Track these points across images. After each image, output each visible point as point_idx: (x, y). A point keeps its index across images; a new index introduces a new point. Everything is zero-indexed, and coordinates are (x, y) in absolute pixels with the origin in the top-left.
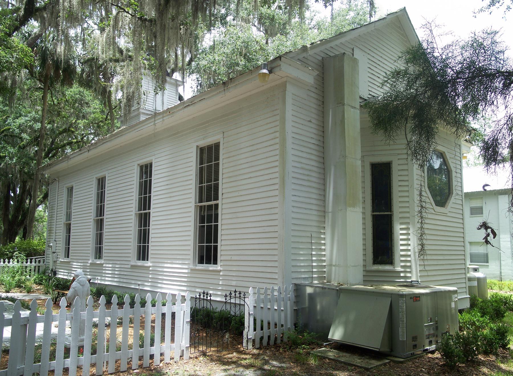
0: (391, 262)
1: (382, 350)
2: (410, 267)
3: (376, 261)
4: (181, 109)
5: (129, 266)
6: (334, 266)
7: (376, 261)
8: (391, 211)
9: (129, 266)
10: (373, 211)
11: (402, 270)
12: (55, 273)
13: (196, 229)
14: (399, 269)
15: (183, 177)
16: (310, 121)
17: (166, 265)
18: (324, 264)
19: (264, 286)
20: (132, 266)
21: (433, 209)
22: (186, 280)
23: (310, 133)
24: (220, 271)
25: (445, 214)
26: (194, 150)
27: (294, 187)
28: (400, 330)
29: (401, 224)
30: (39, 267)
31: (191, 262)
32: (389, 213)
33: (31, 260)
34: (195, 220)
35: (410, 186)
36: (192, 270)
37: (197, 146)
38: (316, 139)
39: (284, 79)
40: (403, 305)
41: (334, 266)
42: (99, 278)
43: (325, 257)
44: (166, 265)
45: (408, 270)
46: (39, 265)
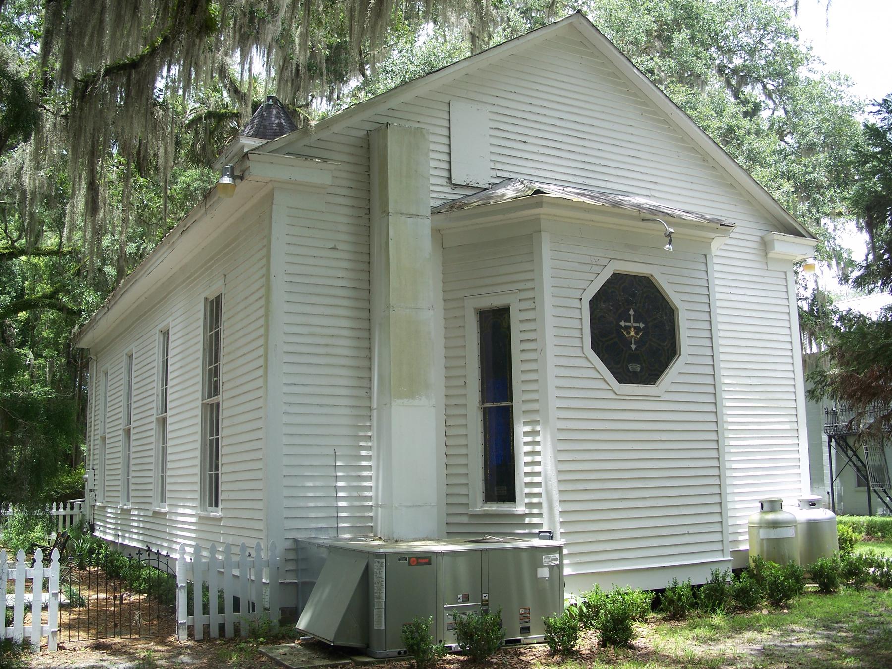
0: (511, 497)
1: (338, 643)
2: (539, 505)
3: (489, 497)
4: (178, 239)
5: (150, 514)
6: (381, 506)
7: (489, 497)
8: (512, 401)
9: (150, 514)
10: (483, 401)
11: (527, 511)
12: (92, 528)
13: (205, 445)
14: (520, 509)
15: (250, 343)
16: (334, 248)
17: (181, 511)
18: (370, 504)
19: (230, 540)
20: (155, 513)
21: (612, 390)
22: (193, 535)
23: (334, 269)
24: (220, 519)
25: (656, 399)
26: (201, 306)
27: (286, 368)
28: (375, 612)
29: (526, 423)
30: (72, 516)
31: (196, 504)
32: (508, 404)
33: (72, 504)
34: (203, 429)
35: (539, 350)
36: (200, 518)
37: (206, 299)
38: (350, 279)
39: (270, 186)
40: (380, 573)
41: (381, 506)
42: (127, 535)
43: (371, 491)
44: (181, 511)
45: (535, 511)
46: (72, 513)
